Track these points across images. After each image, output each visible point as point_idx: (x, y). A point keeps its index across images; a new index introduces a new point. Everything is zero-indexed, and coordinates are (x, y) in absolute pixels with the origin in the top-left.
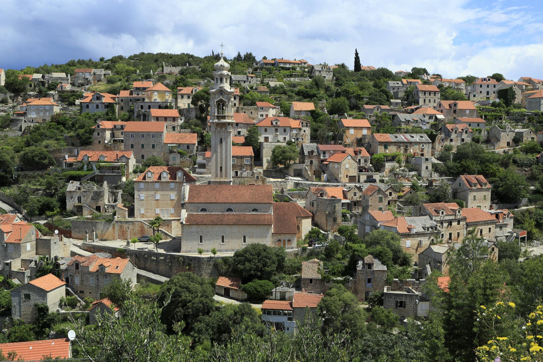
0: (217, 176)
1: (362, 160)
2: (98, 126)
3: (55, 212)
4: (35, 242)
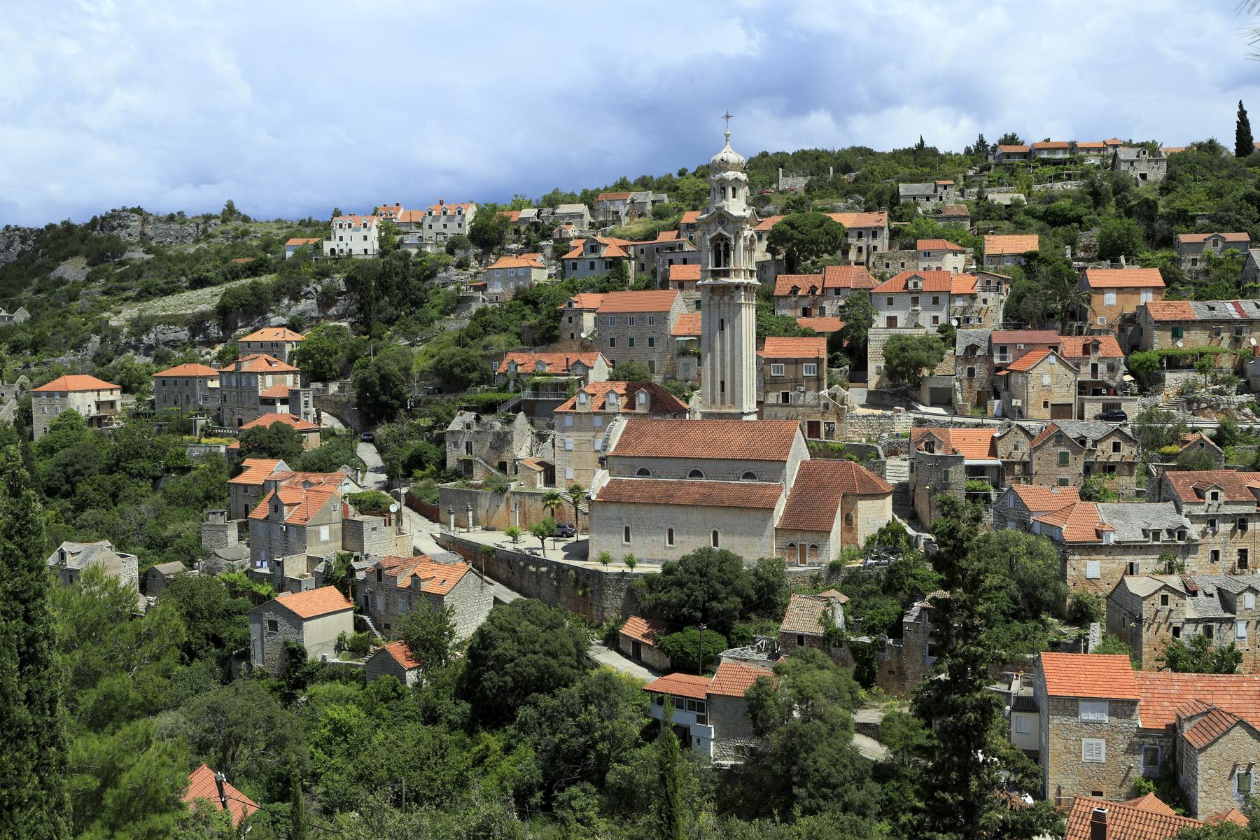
0: (713, 402)
2: (570, 304)
3: (427, 471)
4: (340, 526)
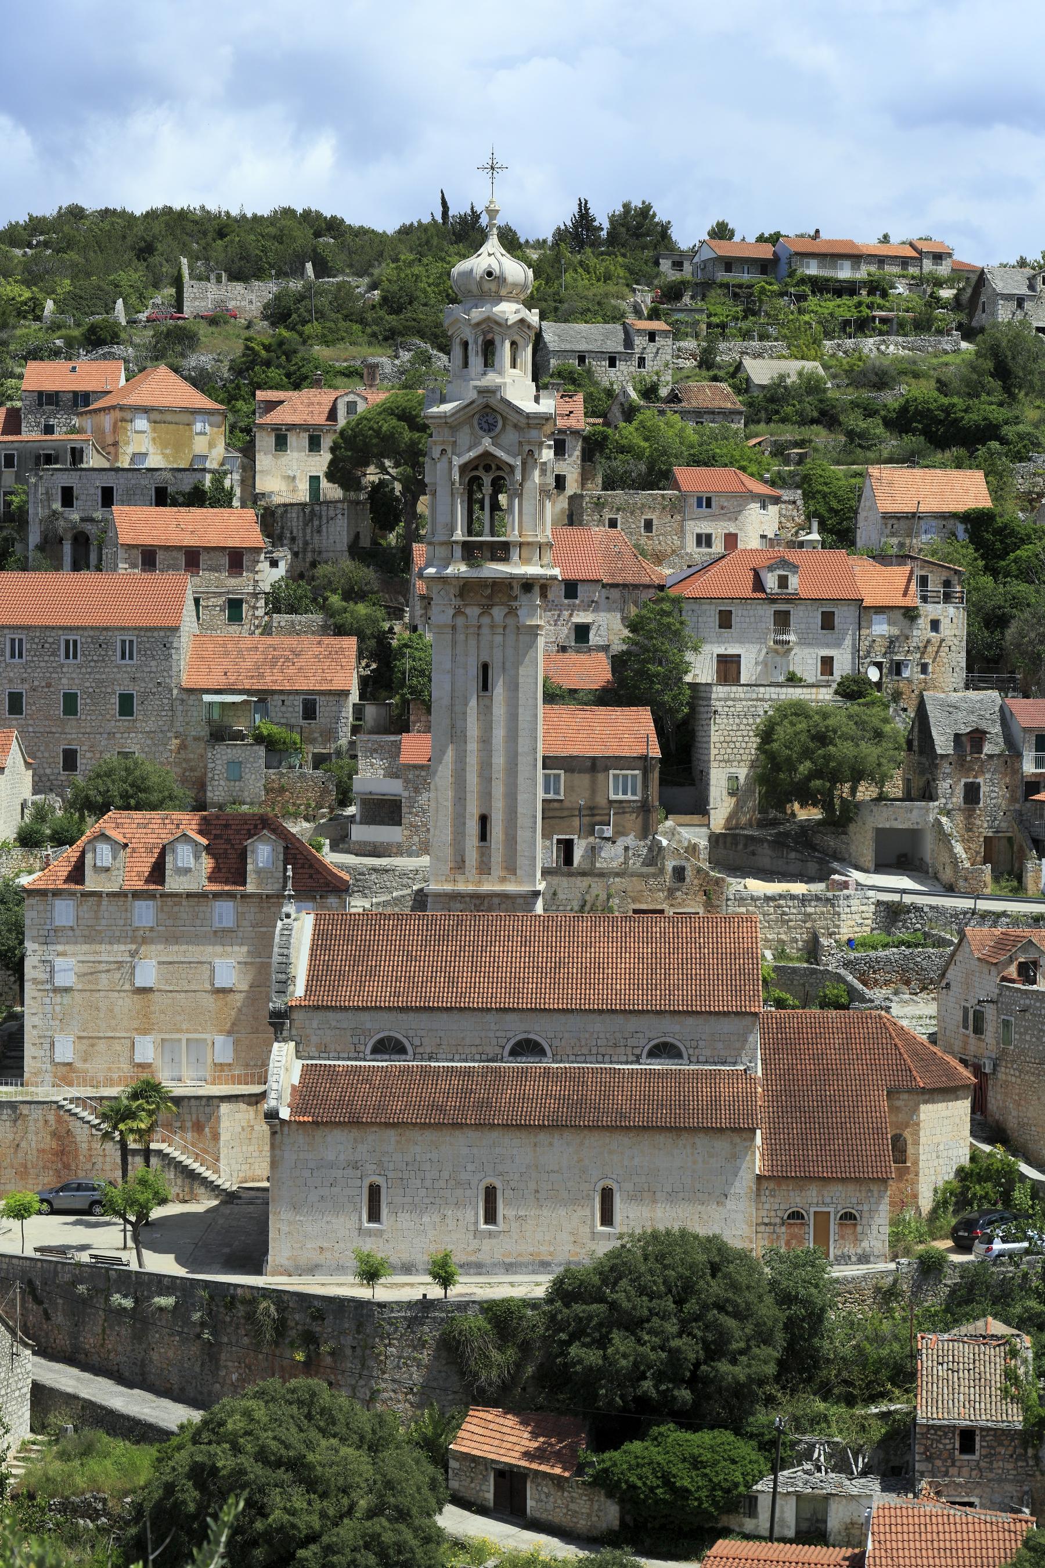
0: (460, 866)
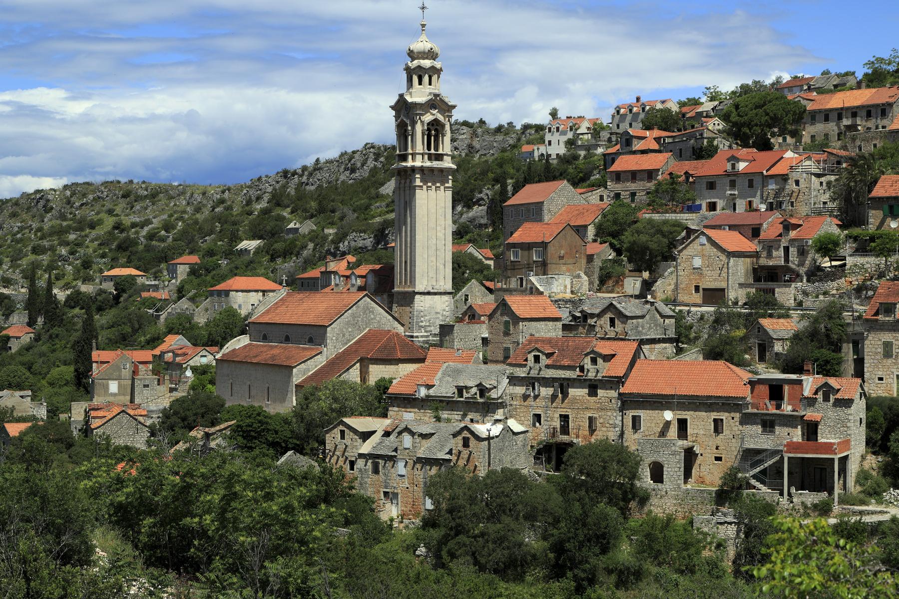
1: (791, 249)
